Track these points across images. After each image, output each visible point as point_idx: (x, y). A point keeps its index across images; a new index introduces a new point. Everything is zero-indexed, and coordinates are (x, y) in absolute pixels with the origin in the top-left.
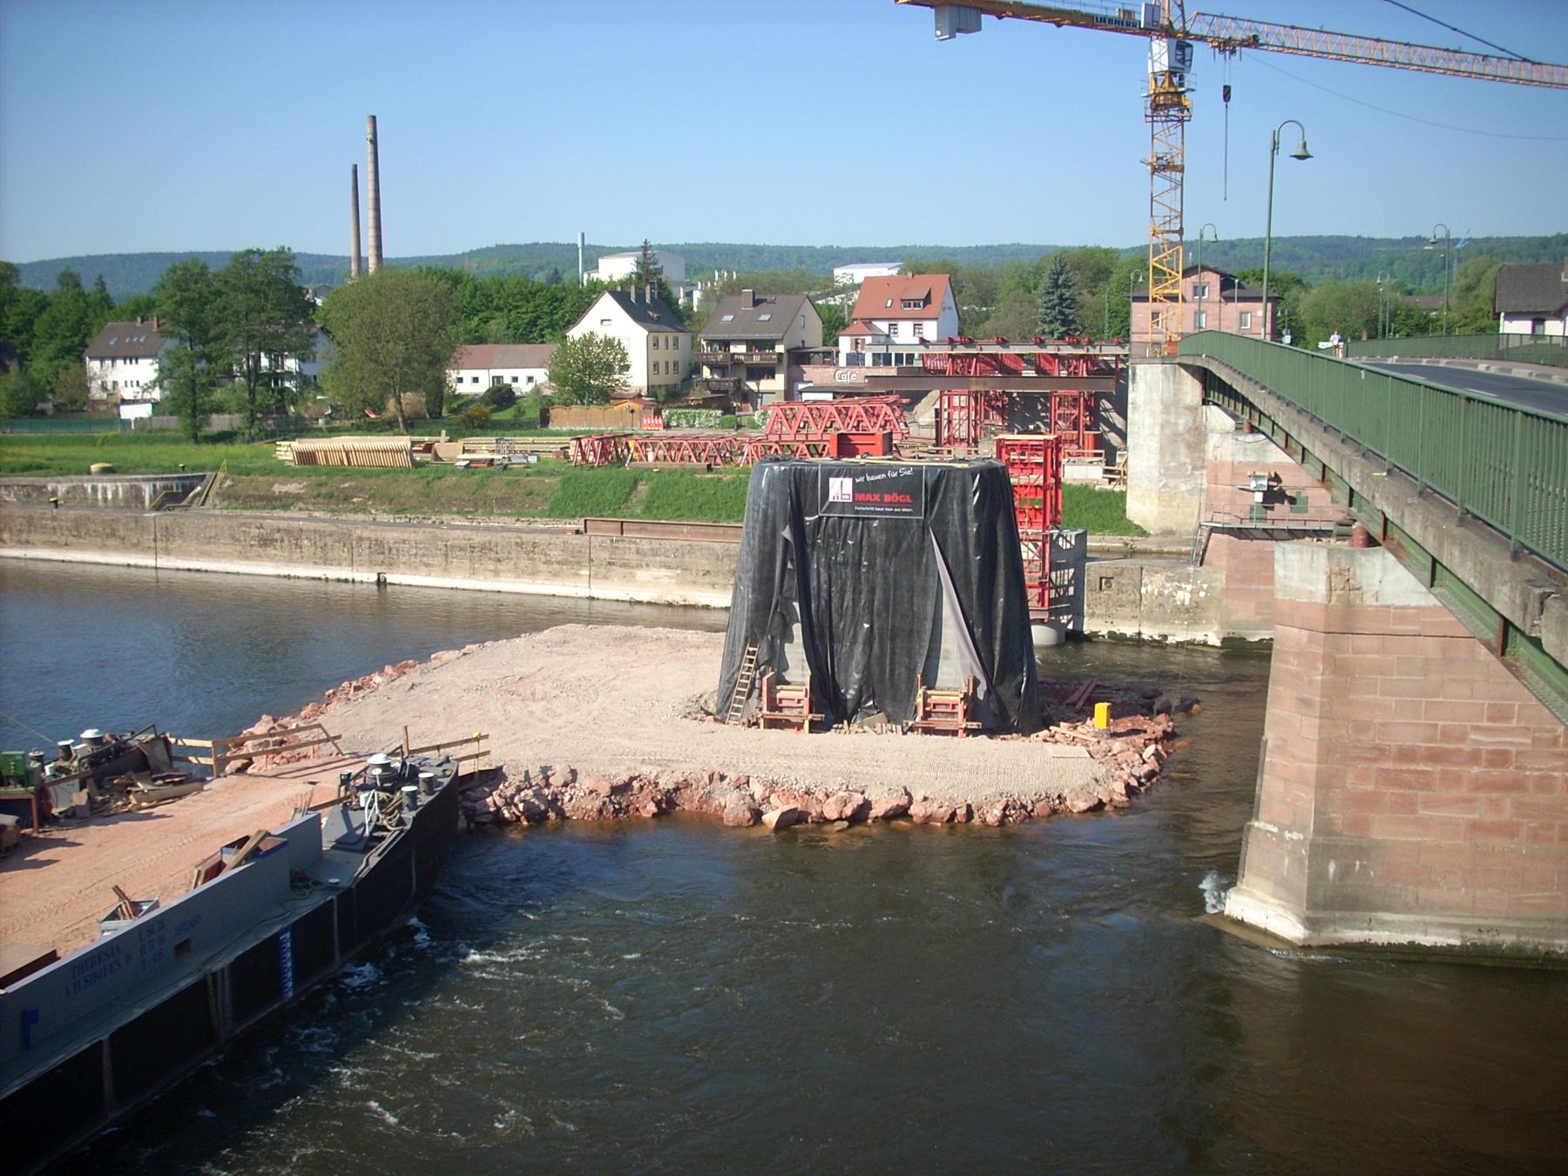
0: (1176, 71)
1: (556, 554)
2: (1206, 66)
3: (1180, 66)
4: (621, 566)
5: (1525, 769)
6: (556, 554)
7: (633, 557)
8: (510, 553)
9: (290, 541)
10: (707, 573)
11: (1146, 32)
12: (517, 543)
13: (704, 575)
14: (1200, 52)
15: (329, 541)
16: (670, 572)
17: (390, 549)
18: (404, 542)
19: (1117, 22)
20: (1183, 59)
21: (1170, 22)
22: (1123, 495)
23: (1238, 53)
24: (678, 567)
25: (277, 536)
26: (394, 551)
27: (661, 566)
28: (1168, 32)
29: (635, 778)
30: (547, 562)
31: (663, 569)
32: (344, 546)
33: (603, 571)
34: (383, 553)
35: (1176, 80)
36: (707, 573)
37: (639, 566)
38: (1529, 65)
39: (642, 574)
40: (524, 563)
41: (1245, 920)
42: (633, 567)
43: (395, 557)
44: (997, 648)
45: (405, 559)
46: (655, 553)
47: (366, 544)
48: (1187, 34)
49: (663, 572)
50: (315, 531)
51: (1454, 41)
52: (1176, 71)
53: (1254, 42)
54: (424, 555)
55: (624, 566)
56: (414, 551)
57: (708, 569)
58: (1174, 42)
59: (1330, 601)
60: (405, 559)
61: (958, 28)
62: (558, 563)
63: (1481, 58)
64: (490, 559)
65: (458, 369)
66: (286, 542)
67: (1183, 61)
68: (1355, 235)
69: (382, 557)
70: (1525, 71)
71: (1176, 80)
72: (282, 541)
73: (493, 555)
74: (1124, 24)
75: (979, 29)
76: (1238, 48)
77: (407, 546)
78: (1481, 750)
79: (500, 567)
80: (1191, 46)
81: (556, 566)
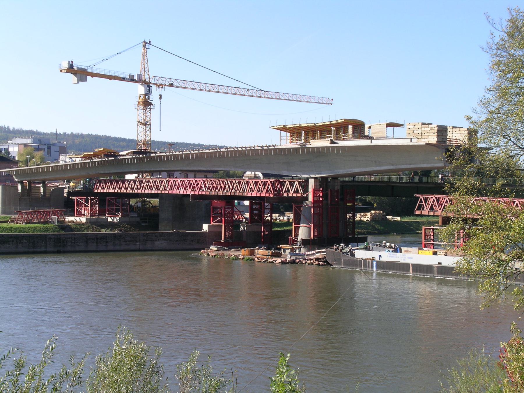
0: (148, 93)
2: (155, 92)
3: (148, 93)
4: (150, 241)
8: (111, 239)
9: (17, 241)
11: (136, 82)
12: (114, 236)
13: (176, 241)
14: (154, 87)
16: (166, 242)
18: (69, 238)
19: (129, 79)
20: (149, 91)
21: (145, 79)
23: (164, 88)
24: (168, 240)
25: (11, 240)
26: (65, 242)
27: (163, 240)
28: (144, 82)
30: (125, 241)
31: (164, 241)
32: (43, 241)
34: (61, 243)
35: (147, 97)
37: (156, 240)
38: (263, 92)
41: (74, 133)
42: (154, 241)
43: (66, 244)
48: (150, 83)
49: (164, 241)
51: (238, 85)
52: (148, 93)
53: (172, 85)
54: (78, 242)
55: (151, 241)
56: (74, 241)
57: (177, 239)
58: (146, 85)
59: (300, 252)
60: (69, 244)
61: (79, 81)
62: (129, 241)
63: (247, 90)
64: (104, 242)
65: (389, 182)
66: (15, 241)
67: (149, 91)
68: (87, 134)
69: (60, 244)
70: (262, 94)
71: (147, 97)
72: (13, 241)
73: (105, 240)
74: (131, 79)
75: (86, 81)
76: (164, 87)
77: (70, 239)
80: (152, 87)
81: (128, 243)
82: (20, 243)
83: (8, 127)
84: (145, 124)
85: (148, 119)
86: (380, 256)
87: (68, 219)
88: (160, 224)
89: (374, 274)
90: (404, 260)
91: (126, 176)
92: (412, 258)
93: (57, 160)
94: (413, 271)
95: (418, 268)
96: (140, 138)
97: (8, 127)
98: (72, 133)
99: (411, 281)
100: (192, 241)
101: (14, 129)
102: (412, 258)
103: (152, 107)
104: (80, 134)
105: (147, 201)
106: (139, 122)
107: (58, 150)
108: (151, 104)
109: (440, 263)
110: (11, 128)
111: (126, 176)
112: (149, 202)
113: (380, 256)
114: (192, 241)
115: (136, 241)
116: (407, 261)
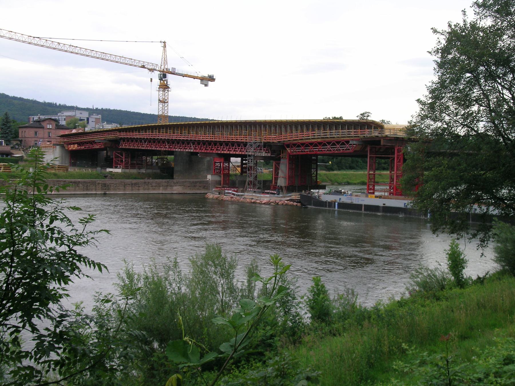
1: (154, 184)
5: (324, 247)
6: (154, 184)
7: (173, 184)
10: (189, 186)
15: (89, 184)
17: (108, 186)
18: (112, 184)
22: (364, 205)
25: (71, 184)
29: (362, 328)
33: (165, 187)
36: (189, 186)
39: (175, 188)
40: (146, 187)
41: (104, 108)
44: (351, 211)
45: (113, 188)
46: (177, 183)
47: (100, 185)
49: (179, 187)
50: (84, 182)
55: (170, 186)
60: (113, 188)
73: (138, 185)
78: (394, 155)
79: (140, 188)
81: (154, 187)
82: (77, 186)
83: (56, 103)
84: (163, 102)
85: (166, 98)
86: (340, 199)
87: (109, 170)
88: (174, 175)
89: (336, 212)
90: (358, 202)
91: (231, 158)
92: (364, 200)
93: (430, 213)
94: (365, 210)
95: (369, 208)
96: (160, 113)
97: (56, 103)
98: (102, 109)
99: (363, 216)
100: (200, 187)
101: (60, 104)
102: (364, 200)
103: (169, 90)
104: (58, 104)
105: (165, 158)
106: (159, 100)
107: (94, 120)
108: (168, 88)
109: (384, 204)
110: (58, 104)
111: (231, 158)
112: (167, 158)
113: (340, 199)
114: (200, 187)
115: (160, 186)
116: (360, 203)
